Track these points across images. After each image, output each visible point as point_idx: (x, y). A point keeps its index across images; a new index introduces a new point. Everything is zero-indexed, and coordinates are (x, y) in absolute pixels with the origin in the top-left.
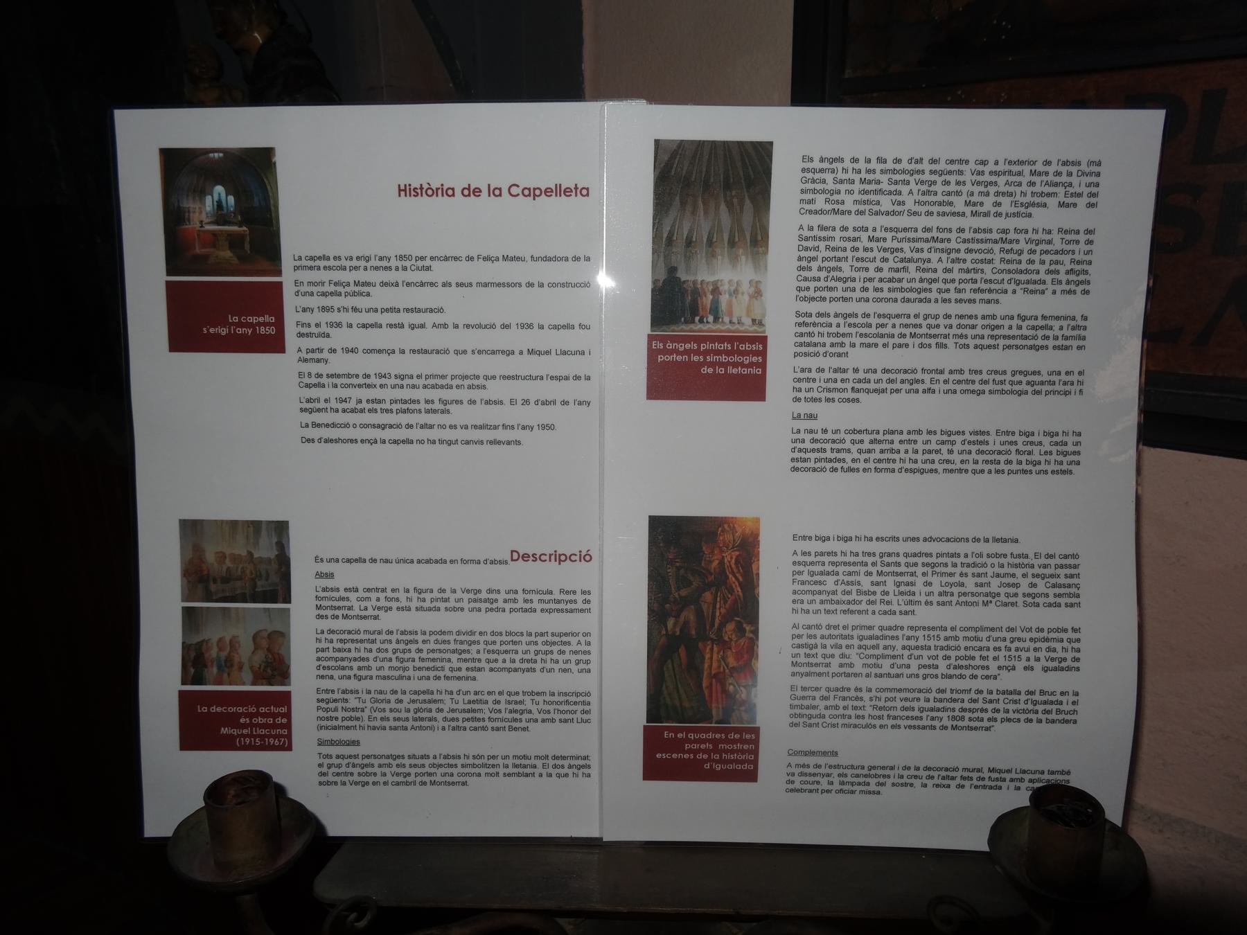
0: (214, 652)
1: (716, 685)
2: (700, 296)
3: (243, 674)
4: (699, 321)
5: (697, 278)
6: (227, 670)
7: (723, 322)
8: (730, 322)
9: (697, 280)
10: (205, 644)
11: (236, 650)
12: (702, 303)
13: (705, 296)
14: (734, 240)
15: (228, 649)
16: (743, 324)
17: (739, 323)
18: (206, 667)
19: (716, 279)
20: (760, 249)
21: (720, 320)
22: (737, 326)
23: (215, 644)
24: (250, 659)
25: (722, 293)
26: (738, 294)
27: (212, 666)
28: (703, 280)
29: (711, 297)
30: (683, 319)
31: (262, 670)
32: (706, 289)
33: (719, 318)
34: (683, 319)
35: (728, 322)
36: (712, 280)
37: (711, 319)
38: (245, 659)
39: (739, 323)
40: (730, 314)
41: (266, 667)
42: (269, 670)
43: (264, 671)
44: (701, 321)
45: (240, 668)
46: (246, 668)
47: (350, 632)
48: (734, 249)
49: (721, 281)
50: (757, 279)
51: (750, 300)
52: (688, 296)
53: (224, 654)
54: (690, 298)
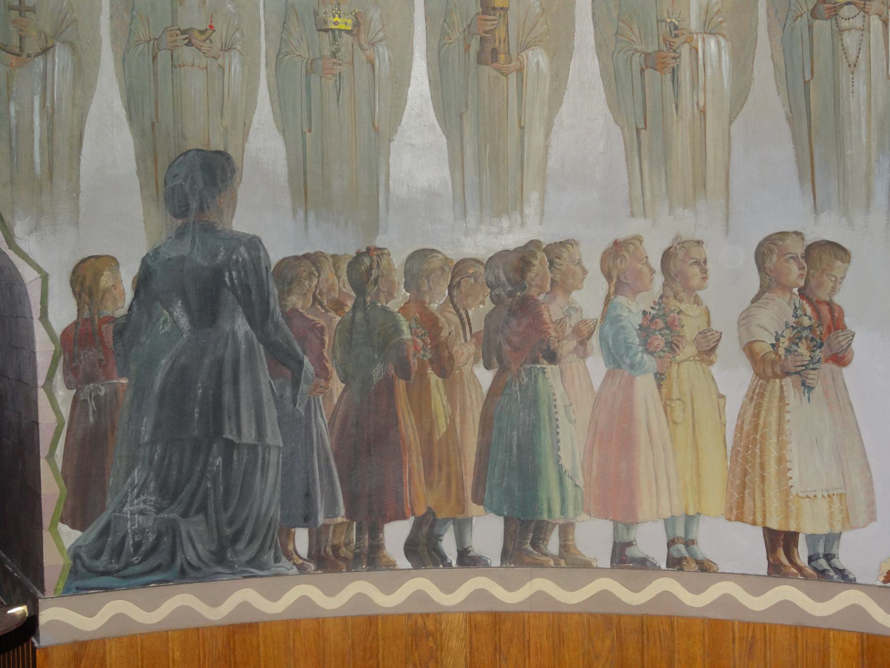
2: (404, 370)
3: (714, 370)
4: (411, 548)
5: (380, 242)
6: (650, 363)
10: (540, 262)
11: (691, 290)
15: (659, 279)
16: (704, 567)
17: (675, 563)
18: (552, 357)
19: (513, 240)
21: (553, 544)
24: (745, 319)
25: (567, 346)
26: (672, 347)
28: (422, 255)
29: (485, 377)
30: (301, 539)
31: (782, 351)
32: (449, 322)
33: (540, 531)
34: (301, 539)
35: (605, 561)
36: (484, 255)
39: (675, 563)
41: (795, 340)
42: (803, 349)
43: (787, 350)
47: (781, 460)
50: (816, 232)
51: (756, 397)
52: (323, 373)
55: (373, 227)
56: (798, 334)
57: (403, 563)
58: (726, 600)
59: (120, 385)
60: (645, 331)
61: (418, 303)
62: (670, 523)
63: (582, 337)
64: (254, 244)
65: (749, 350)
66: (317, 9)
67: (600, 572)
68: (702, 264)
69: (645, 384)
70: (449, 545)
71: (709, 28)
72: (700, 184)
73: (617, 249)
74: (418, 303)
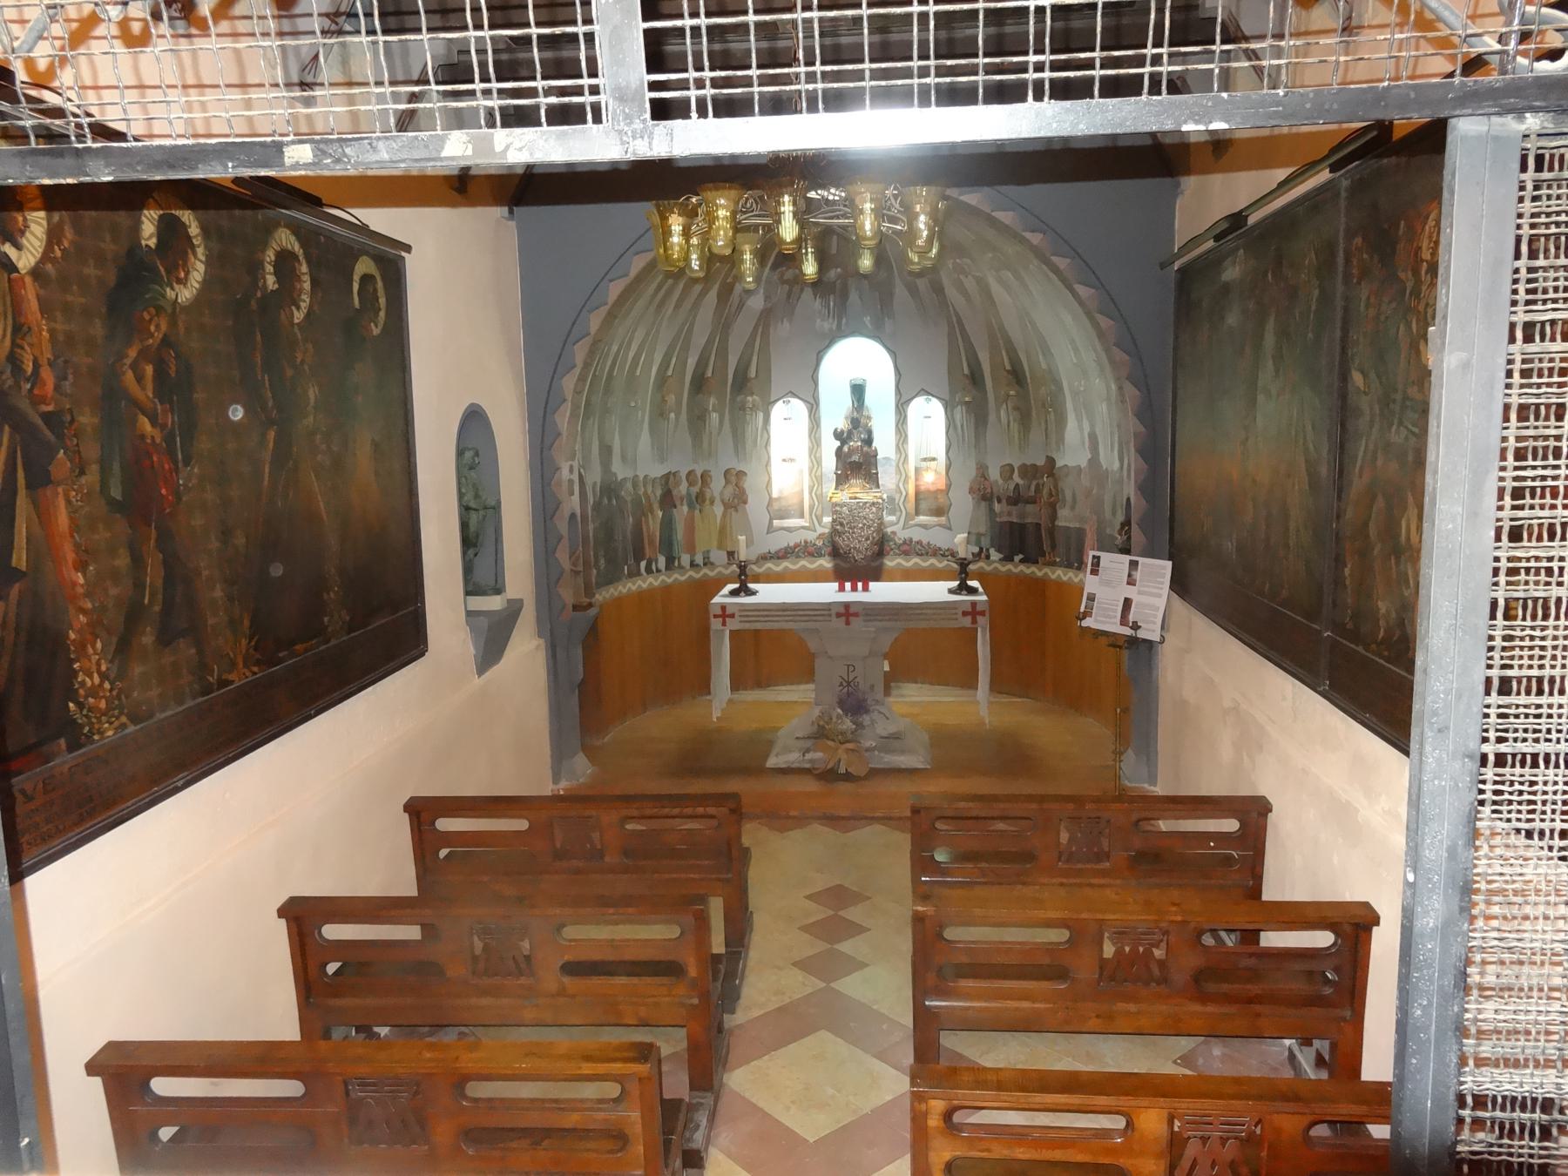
0: (683, 488)
1: (998, 411)
5: (638, 473)
6: (698, 506)
7: (680, 567)
8: (693, 565)
9: (637, 476)
10: (671, 476)
12: (648, 529)
13: (652, 513)
14: (703, 374)
16: (712, 564)
17: (705, 564)
18: (675, 507)
20: (749, 398)
21: (676, 564)
22: (706, 571)
23: (684, 478)
24: (721, 493)
25: (678, 503)
26: (704, 501)
27: (682, 505)
29: (660, 514)
33: (674, 558)
35: (688, 567)
37: (662, 561)
38: (716, 495)
40: (691, 549)
44: (649, 570)
45: (712, 503)
46: (718, 501)
48: (700, 396)
49: (674, 474)
50: (738, 469)
51: (724, 515)
53: (695, 490)
54: (631, 519)
55: (636, 469)
56: (735, 496)
57: (645, 574)
58: (720, 572)
59: (163, 205)
60: (697, 498)
61: (645, 493)
62: (704, 553)
63: (682, 499)
64: (615, 474)
65: (723, 501)
66: (1233, 10)
67: (688, 571)
68: (710, 477)
69: (697, 512)
70: (654, 568)
71: (714, 411)
72: (710, 454)
73: (690, 473)
74: (645, 493)
